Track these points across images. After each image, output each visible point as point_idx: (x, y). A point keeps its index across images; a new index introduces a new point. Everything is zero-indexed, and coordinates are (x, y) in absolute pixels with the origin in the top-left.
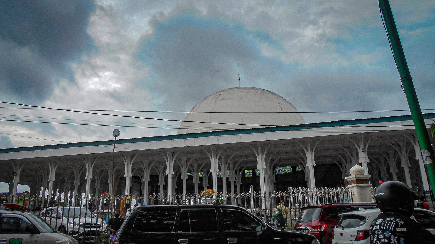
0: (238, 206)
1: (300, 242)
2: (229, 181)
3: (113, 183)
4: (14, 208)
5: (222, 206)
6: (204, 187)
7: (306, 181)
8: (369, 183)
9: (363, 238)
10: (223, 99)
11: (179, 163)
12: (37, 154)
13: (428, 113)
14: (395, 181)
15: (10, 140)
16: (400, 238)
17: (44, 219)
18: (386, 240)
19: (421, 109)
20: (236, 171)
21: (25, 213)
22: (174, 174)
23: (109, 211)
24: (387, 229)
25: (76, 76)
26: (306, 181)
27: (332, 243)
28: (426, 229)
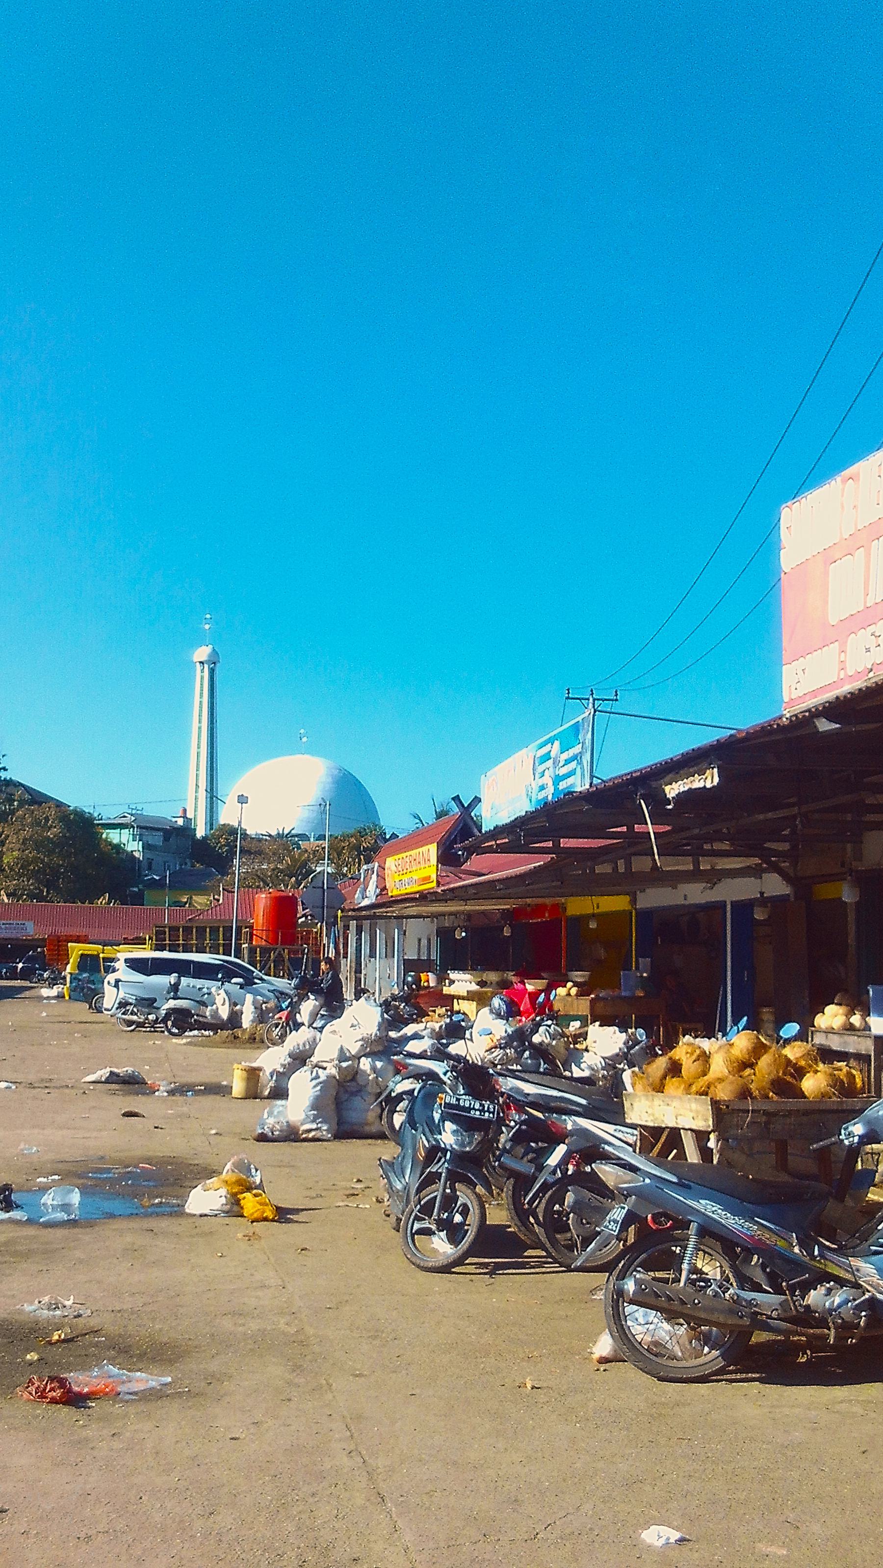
0: (166, 955)
1: (534, 1142)
2: (465, 994)
3: (410, 905)
4: (213, 1366)
5: (427, 1202)
6: (832, 1064)
7: (313, 1109)
8: (230, 956)
9: (227, 1399)
10: (224, 1001)
11: (278, 1029)
12: (687, 1053)
13: (585, 1276)
14: (232, 959)
15: (432, 1246)
16: (457, 1223)
17: (594, 779)
18: (460, 1079)
19: (122, 831)
20: (766, 1293)
21: (315, 1087)
22: (643, 1536)
23: (628, 865)
24: (807, 1275)
25: (694, 1106)
26: (313, 1109)
27: (873, 678)
28: (838, 726)
